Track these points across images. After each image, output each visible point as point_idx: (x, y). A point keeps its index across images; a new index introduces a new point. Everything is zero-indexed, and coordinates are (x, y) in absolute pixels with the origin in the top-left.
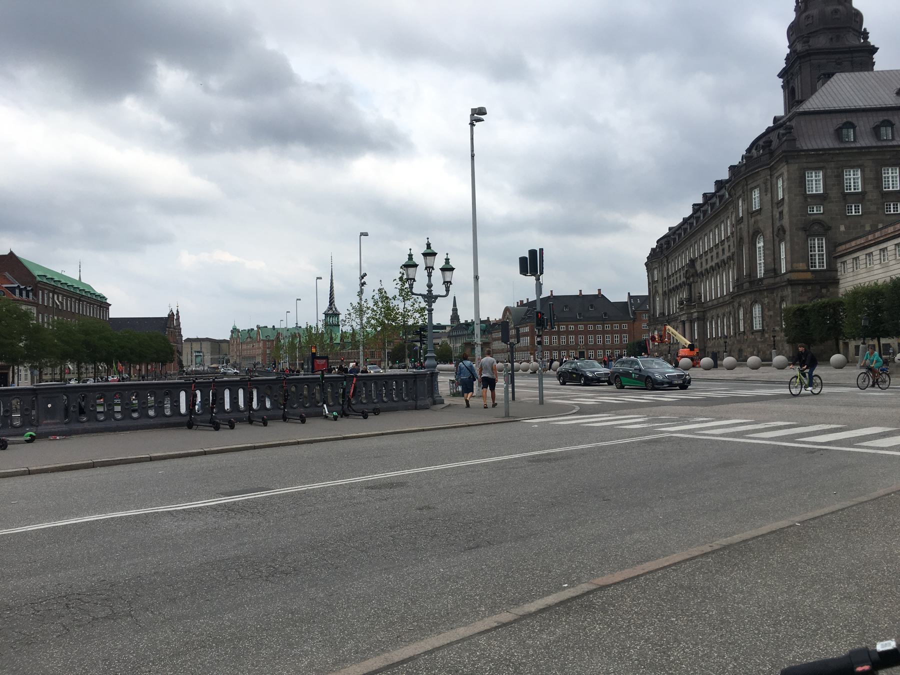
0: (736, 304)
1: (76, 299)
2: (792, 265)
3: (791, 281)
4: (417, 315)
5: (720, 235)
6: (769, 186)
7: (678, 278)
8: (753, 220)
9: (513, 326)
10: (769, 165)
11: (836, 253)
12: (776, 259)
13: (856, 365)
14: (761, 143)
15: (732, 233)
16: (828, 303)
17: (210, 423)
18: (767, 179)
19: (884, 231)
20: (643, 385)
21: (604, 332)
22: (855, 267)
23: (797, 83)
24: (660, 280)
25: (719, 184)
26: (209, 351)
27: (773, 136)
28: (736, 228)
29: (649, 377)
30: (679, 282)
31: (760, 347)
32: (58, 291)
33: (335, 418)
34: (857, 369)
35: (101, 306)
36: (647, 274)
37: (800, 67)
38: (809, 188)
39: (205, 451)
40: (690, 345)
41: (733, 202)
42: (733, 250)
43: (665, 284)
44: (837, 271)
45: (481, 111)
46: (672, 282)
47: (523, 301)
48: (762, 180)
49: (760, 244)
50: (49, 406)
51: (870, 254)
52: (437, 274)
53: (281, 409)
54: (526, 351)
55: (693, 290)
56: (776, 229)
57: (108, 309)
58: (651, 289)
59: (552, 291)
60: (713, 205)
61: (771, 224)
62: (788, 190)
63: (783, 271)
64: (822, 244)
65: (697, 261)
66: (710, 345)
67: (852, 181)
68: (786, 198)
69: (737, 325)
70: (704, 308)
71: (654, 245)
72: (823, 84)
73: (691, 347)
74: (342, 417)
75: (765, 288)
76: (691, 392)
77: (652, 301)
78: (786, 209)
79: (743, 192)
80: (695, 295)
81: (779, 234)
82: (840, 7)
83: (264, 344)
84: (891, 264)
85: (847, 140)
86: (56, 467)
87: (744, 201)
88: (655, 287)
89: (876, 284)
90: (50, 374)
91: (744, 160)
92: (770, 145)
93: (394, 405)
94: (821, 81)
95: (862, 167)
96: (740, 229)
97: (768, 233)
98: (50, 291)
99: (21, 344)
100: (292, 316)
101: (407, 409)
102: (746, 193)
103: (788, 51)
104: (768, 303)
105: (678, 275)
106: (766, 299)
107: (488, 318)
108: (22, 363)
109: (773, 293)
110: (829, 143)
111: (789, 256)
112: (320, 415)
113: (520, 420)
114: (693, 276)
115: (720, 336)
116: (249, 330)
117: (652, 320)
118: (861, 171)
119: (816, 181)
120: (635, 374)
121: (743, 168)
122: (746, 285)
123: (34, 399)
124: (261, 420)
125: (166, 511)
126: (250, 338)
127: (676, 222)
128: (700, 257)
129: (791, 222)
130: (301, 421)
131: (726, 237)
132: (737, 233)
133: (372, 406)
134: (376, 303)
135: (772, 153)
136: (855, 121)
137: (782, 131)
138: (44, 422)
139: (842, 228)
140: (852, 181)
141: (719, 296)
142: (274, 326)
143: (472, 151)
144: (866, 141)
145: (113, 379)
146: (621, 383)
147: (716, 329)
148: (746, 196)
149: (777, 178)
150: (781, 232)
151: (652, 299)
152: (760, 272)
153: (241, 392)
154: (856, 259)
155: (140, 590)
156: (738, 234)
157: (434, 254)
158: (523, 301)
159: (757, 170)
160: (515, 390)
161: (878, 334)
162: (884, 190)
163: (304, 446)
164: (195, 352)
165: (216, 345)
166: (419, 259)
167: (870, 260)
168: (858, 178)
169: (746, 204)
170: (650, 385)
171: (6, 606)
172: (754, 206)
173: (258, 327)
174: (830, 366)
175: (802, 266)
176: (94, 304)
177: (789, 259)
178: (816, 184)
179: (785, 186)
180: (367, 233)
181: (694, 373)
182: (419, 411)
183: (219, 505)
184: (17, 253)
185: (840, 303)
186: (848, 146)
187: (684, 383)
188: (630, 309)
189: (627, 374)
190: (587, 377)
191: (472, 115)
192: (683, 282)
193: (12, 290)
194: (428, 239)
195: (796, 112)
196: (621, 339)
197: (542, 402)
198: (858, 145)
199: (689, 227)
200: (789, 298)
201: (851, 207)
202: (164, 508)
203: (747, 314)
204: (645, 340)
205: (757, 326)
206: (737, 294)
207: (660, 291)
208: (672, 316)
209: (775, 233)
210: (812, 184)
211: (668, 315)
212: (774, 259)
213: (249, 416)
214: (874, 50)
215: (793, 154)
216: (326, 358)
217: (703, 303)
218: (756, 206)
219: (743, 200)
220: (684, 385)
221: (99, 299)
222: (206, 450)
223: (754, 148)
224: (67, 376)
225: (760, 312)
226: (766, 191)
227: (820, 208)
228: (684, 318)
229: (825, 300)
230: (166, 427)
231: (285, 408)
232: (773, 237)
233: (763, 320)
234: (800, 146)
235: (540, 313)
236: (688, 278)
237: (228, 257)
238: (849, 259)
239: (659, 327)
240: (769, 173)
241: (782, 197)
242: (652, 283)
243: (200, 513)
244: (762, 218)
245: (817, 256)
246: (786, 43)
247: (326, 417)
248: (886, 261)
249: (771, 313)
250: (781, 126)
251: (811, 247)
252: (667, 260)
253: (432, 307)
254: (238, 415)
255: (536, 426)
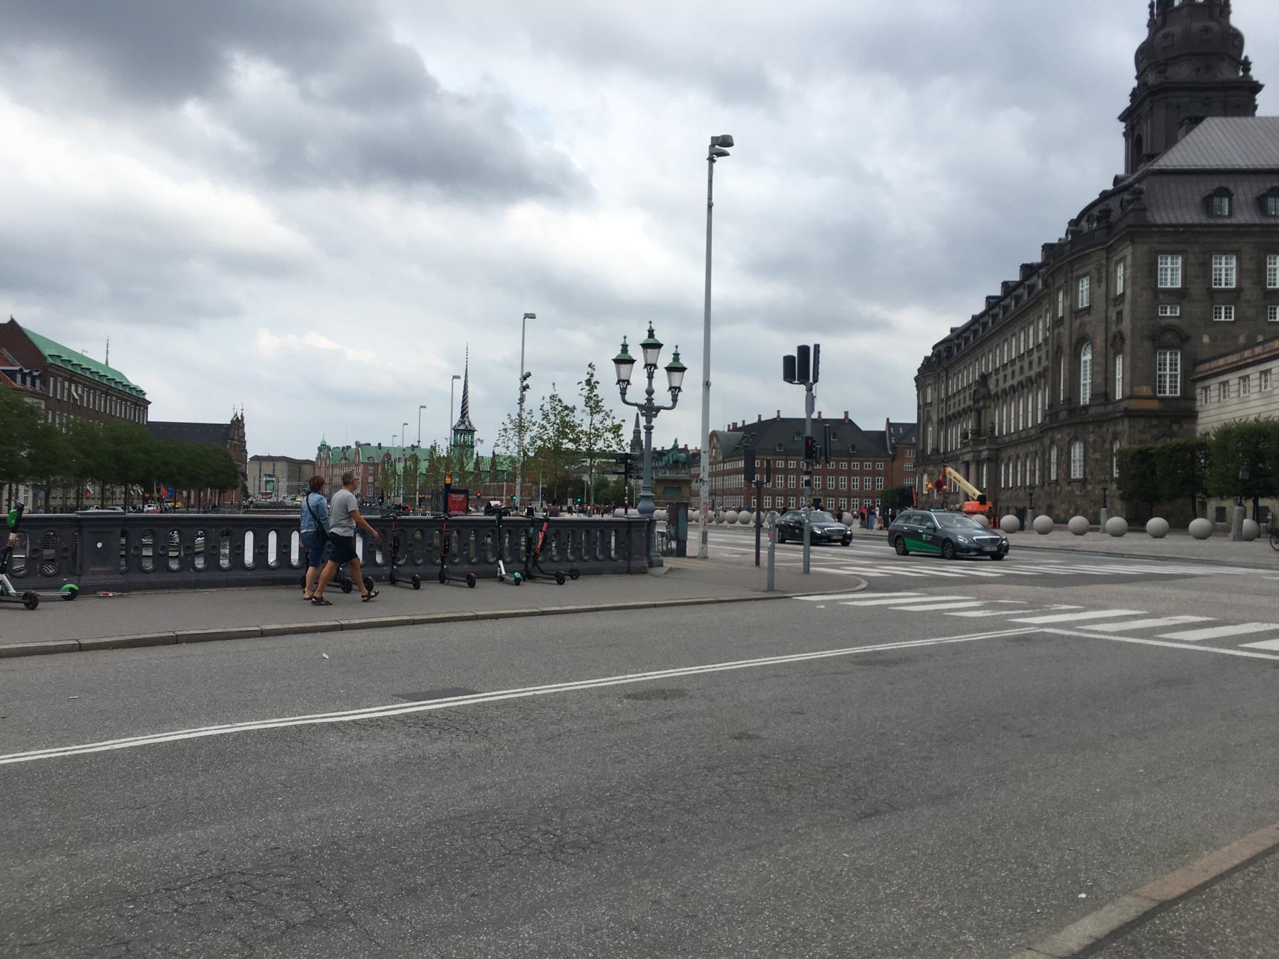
0: (1047, 441)
1: (102, 392)
2: (1131, 389)
3: (1129, 411)
4: (610, 435)
5: (1026, 341)
6: (1104, 275)
7: (962, 401)
8: (1078, 322)
9: (721, 458)
10: (1105, 243)
11: (1197, 374)
12: (1109, 379)
13: (1227, 536)
14: (1095, 212)
15: (1046, 340)
16: (1184, 444)
17: (335, 581)
18: (1101, 265)
19: (1268, 346)
20: (938, 551)
21: (850, 473)
22: (1222, 395)
23: (1145, 130)
24: (935, 401)
25: (1028, 270)
26: (285, 475)
27: (1114, 204)
28: (1053, 333)
29: (948, 540)
30: (962, 406)
31: (1079, 503)
32: (77, 379)
33: (517, 582)
34: (1229, 541)
35: (136, 404)
36: (916, 392)
37: (1151, 108)
38: (1161, 279)
39: (342, 625)
40: (979, 497)
41: (1048, 295)
42: (1044, 363)
43: (942, 408)
44: (1194, 399)
45: (726, 141)
46: (952, 406)
47: (736, 424)
48: (1094, 265)
49: (1087, 357)
50: (99, 545)
51: (1245, 378)
52: (661, 376)
53: (437, 565)
54: (738, 495)
55: (983, 418)
56: (1110, 336)
57: (147, 408)
58: (922, 415)
59: (779, 412)
60: (1018, 298)
61: (1104, 328)
62: (1132, 281)
63: (1119, 396)
64: (1176, 360)
65: (991, 377)
66: (1004, 497)
67: (1223, 272)
68: (1128, 292)
69: (1047, 473)
70: (999, 445)
71: (929, 353)
72: (1187, 132)
73: (982, 500)
74: (524, 580)
75: (1091, 419)
76: (1014, 564)
77: (921, 432)
78: (1127, 308)
79: (1066, 282)
80: (985, 425)
81: (1115, 343)
82: (1213, 24)
83: (366, 469)
84: (1251, 398)
85: (1219, 213)
86: (121, 641)
87: (1067, 294)
88: (928, 411)
89: (1256, 420)
90: (61, 498)
91: (1070, 236)
92: (1109, 216)
93: (597, 565)
94: (1184, 127)
95: (1236, 252)
96: (1059, 333)
97: (1099, 341)
98: (65, 379)
99: (22, 453)
100: (413, 426)
101: (616, 572)
102: (1070, 283)
103: (1135, 83)
104: (1094, 441)
105: (962, 397)
106: (1091, 436)
107: (686, 446)
108: (21, 481)
109: (1102, 427)
110: (1192, 216)
111: (1128, 375)
112: (493, 576)
113: (791, 597)
114: (984, 398)
115: (1019, 484)
116: (343, 448)
117: (920, 459)
118: (1237, 259)
119: (1172, 270)
120: (927, 534)
121: (1067, 248)
122: (1063, 415)
123: (76, 534)
124: (411, 580)
125: (328, 723)
126: (346, 459)
127: (961, 320)
128: (995, 371)
129: (1132, 330)
130: (469, 584)
131: (1036, 344)
132: (1053, 340)
133: (569, 566)
134: (546, 416)
135: (1110, 227)
136: (1231, 187)
137: (1126, 196)
138: (91, 569)
139: (1206, 339)
140: (1223, 272)
141: (1021, 429)
142: (380, 444)
143: (710, 198)
144: (1246, 216)
145: (151, 510)
146: (905, 546)
147: (1010, 476)
148: (1069, 287)
149: (1117, 263)
150: (1118, 341)
151: (921, 429)
152: (1085, 397)
153: (273, 538)
154: (1225, 383)
155: (345, 869)
156: (1055, 341)
157: (659, 346)
158: (736, 424)
159: (1088, 251)
160: (761, 551)
161: (1257, 492)
162: (1268, 287)
163: (488, 623)
164: (266, 475)
165: (295, 466)
166: (636, 352)
167: (1244, 386)
168: (1231, 269)
169: (1069, 298)
170: (949, 552)
171: (123, 892)
172: (1080, 302)
173: (358, 444)
174: (1189, 535)
175: (1146, 390)
176: (126, 401)
177: (1128, 380)
178: (1172, 275)
179: (1127, 276)
180: (534, 315)
181: (1014, 539)
182: (633, 576)
183: (408, 715)
184: (22, 323)
185: (1202, 445)
186: (1220, 221)
187: (999, 549)
188: (888, 441)
189: (914, 535)
190: (813, 534)
191: (712, 146)
192: (969, 407)
193: (12, 374)
194: (650, 323)
195: (1149, 171)
196: (874, 483)
197: (806, 570)
198: (1234, 221)
199: (981, 329)
200: (1126, 435)
201: (1220, 309)
202: (322, 718)
203: (1062, 455)
204: (911, 487)
205: (1077, 472)
206: (1049, 426)
207: (935, 419)
208: (951, 454)
209: (1110, 342)
210: (1166, 275)
211: (945, 453)
212: (1106, 379)
213: (391, 574)
214: (1257, 87)
215: (1141, 231)
216: (466, 492)
217: (997, 438)
218: (1083, 302)
219: (1065, 293)
220: (998, 553)
221: (135, 394)
222: (343, 622)
223: (1085, 218)
224: (86, 503)
225: (1082, 454)
226: (1099, 281)
227: (1176, 308)
228: (968, 457)
229: (1181, 441)
230: (269, 585)
231: (443, 563)
232: (1106, 347)
233: (1085, 466)
234: (1151, 218)
235: (811, 438)
236: (976, 401)
237: (320, 342)
238: (1214, 384)
239: (930, 469)
240: (1105, 256)
241: (1122, 291)
242: (923, 407)
243: (382, 728)
244: (1091, 319)
245: (1168, 377)
246: (1133, 72)
247: (502, 579)
248: (1269, 389)
249: (1098, 456)
250: (1126, 188)
251: (1160, 364)
252: (947, 375)
253: (652, 424)
254: (375, 571)
255: (822, 607)
